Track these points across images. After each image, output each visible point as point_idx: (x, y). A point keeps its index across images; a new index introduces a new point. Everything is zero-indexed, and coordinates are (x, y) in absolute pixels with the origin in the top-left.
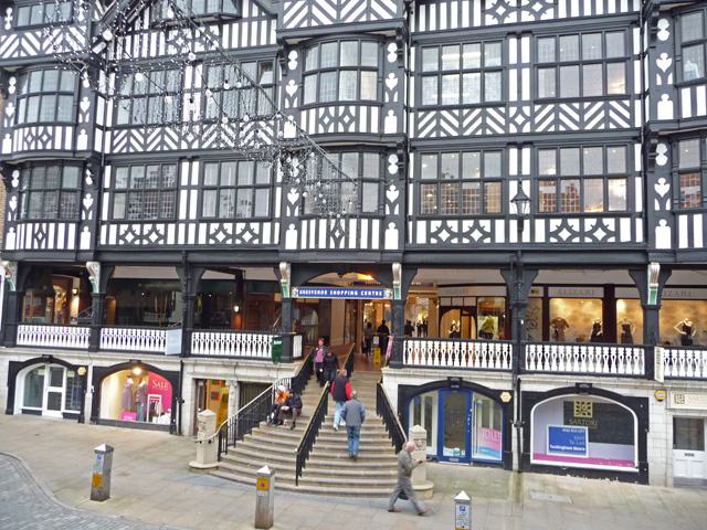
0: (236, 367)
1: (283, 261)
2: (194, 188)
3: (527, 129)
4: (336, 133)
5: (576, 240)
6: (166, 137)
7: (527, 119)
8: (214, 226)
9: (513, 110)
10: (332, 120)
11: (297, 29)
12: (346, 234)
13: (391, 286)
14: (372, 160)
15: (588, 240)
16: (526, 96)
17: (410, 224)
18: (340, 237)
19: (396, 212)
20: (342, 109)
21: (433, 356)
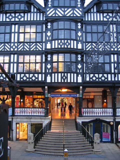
0: (30, 119)
1: (46, 86)
2: (15, 63)
3: (16, 50)
4: (64, 48)
5: (97, 80)
6: (37, 46)
7: (16, 47)
8: (22, 75)
9: (12, 44)
10: (63, 44)
11: (51, 16)
12: (67, 78)
13: (79, 93)
14: (73, 56)
15: (100, 80)
16: (16, 41)
17: (85, 75)
18: (65, 79)
19: (81, 71)
20: (66, 41)
21: (104, 113)
